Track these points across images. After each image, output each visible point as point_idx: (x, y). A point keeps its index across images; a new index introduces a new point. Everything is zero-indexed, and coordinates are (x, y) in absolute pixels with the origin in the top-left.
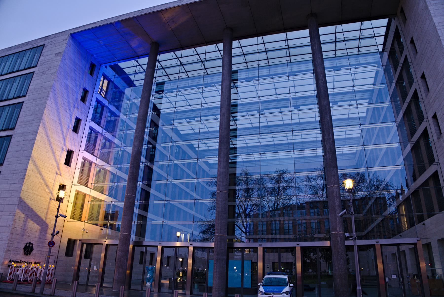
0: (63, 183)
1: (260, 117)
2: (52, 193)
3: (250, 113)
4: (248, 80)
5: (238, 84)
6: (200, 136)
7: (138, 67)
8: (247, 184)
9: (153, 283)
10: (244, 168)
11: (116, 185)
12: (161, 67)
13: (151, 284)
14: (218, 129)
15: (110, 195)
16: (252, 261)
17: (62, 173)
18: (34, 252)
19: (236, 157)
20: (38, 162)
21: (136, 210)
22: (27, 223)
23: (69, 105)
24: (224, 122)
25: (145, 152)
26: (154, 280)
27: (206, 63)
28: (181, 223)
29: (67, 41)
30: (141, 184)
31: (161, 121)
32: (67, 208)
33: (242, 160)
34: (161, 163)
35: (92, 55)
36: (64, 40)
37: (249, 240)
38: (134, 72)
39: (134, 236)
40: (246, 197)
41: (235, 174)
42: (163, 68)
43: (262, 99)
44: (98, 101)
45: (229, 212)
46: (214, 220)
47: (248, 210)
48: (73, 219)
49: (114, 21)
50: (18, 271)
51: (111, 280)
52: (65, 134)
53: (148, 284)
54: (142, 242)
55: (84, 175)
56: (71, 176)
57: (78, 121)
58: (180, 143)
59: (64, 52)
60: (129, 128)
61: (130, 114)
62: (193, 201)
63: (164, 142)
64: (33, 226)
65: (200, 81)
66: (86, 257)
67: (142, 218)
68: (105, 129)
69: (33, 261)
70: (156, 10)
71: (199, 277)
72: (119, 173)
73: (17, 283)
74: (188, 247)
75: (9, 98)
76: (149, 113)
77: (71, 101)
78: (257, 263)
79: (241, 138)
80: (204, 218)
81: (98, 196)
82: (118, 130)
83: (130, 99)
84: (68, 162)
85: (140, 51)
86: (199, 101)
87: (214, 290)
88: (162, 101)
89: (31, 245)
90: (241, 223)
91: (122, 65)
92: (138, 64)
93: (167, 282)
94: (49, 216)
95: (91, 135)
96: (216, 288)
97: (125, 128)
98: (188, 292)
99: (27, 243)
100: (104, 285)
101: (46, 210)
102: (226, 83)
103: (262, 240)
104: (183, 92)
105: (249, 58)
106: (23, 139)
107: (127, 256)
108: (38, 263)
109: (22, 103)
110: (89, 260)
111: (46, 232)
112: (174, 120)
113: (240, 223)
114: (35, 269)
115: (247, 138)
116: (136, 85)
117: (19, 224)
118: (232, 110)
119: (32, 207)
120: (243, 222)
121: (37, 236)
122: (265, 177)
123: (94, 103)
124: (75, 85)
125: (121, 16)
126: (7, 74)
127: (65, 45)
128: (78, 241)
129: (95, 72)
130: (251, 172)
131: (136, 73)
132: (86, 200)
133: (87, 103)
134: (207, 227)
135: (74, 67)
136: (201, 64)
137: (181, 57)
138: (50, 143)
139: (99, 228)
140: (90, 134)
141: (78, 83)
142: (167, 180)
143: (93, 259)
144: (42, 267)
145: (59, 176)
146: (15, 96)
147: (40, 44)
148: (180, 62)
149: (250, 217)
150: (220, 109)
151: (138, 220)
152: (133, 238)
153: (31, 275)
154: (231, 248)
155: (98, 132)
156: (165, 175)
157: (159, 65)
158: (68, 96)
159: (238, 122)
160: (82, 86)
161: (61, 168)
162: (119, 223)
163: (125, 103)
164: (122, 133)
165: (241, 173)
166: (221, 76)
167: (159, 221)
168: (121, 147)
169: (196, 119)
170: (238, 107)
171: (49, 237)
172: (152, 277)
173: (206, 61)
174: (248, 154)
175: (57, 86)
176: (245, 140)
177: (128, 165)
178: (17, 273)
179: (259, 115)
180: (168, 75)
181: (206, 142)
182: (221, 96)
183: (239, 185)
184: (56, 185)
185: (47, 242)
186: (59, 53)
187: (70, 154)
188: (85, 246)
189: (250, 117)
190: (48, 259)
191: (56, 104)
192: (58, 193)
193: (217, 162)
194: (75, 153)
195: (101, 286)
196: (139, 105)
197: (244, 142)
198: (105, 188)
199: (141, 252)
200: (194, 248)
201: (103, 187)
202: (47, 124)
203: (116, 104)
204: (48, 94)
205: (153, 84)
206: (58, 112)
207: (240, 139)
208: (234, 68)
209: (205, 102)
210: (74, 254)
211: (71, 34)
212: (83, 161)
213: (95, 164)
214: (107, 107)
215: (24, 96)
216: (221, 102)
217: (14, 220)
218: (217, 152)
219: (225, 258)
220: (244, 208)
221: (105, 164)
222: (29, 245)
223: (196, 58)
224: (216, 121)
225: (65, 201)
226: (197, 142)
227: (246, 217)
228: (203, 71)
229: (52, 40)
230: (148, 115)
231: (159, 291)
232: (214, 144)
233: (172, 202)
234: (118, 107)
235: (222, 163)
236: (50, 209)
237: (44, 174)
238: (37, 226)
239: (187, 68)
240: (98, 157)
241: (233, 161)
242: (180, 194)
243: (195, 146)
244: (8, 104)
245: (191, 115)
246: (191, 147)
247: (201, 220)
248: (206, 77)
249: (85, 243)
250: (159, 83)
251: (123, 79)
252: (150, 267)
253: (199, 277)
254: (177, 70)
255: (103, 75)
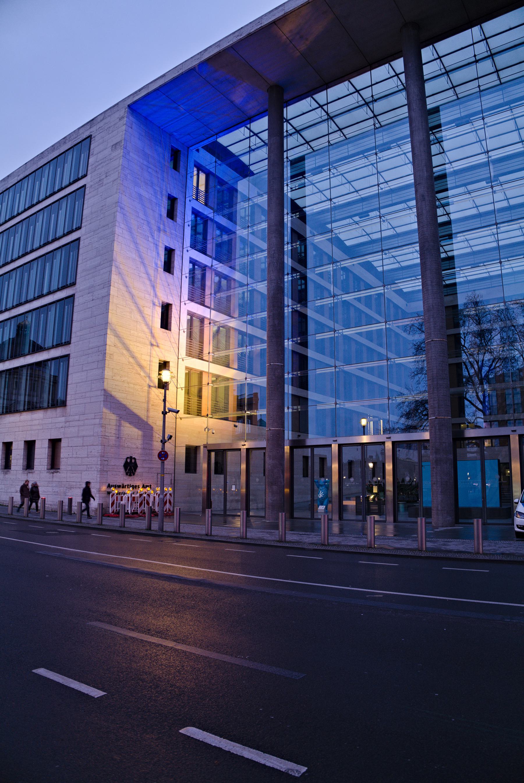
0: (163, 359)
1: (494, 192)
2: (149, 377)
3: (471, 187)
4: (459, 122)
5: (444, 134)
6: (382, 245)
7: (253, 139)
8: (479, 323)
9: (330, 506)
10: (470, 294)
11: (248, 350)
12: (294, 131)
13: (326, 508)
14: (415, 226)
15: (241, 368)
16: (499, 461)
17: (159, 341)
18: (139, 470)
19: (454, 274)
20: (120, 330)
21: (289, 389)
22: (122, 427)
23: (151, 228)
24: (424, 212)
25: (290, 288)
26: (330, 502)
27: (376, 104)
28: (366, 403)
29: (125, 119)
30: (290, 343)
31: (308, 229)
32: (177, 397)
33: (465, 279)
34: (319, 303)
35: (171, 135)
36: (121, 119)
37: (490, 423)
38: (248, 150)
39: (290, 432)
40: (479, 346)
41: (457, 306)
42: (298, 132)
43: (494, 155)
44: (196, 213)
45: (452, 376)
46: (425, 392)
47: (485, 369)
48: (189, 414)
49: (196, 63)
50: (122, 500)
51: (260, 505)
52: (153, 279)
53: (322, 508)
54: (304, 441)
55: (194, 341)
56: (174, 345)
57: (169, 252)
58: (347, 263)
59: (125, 139)
60: (256, 250)
61: (254, 225)
62: (384, 363)
63: (318, 264)
64: (131, 431)
65: (369, 142)
66: (216, 472)
67: (301, 401)
68: (215, 259)
69: (137, 483)
70: (265, 22)
71: (408, 492)
72: (250, 330)
73: (125, 517)
74: (383, 443)
75: (57, 236)
76: (285, 217)
77: (153, 222)
78: (508, 466)
79: (460, 238)
80: (405, 391)
81: (222, 373)
82: (237, 256)
83: (249, 199)
84: (165, 324)
85: (251, 108)
86: (373, 180)
87: (434, 512)
88: (305, 192)
89: (133, 461)
90: (474, 394)
91: (224, 140)
92: (252, 134)
93: (351, 503)
94: (151, 414)
95: (194, 273)
96: (438, 510)
97: (248, 250)
98: (390, 518)
99: (128, 458)
100: (251, 514)
101: (146, 405)
102: (420, 136)
103: (515, 422)
104: (340, 169)
105: (457, 77)
106: (91, 298)
107: (282, 465)
108: (147, 486)
109: (78, 239)
110: (222, 476)
111: (152, 438)
112: (331, 222)
113: (471, 394)
114: (145, 495)
115: (470, 235)
116: (255, 172)
117: (111, 430)
118: (438, 186)
119: (125, 402)
120: (477, 393)
121: (140, 446)
122: (512, 306)
123: (189, 217)
124: (152, 193)
125: (206, 50)
126: (25, 210)
127: (124, 127)
128: (202, 447)
129: (182, 164)
130: (484, 298)
131: (251, 150)
132: (205, 380)
133: (179, 220)
134: (413, 406)
135: (145, 163)
136: (365, 108)
137: (327, 104)
138: (132, 296)
139: (230, 424)
140: (192, 272)
141: (158, 189)
142: (335, 331)
143: (228, 474)
144: (155, 491)
145: (156, 348)
146: (66, 232)
147: (85, 137)
148: (327, 113)
149: (489, 382)
150: (414, 189)
151: (292, 405)
152: (289, 435)
153: (141, 504)
154: (459, 439)
155: (206, 266)
156: (330, 323)
157: (290, 127)
158: (145, 214)
159: (451, 209)
160: (164, 192)
161: (156, 335)
162: (261, 412)
163: (242, 208)
164: (245, 260)
165: (465, 304)
166: (408, 125)
167: (329, 404)
168: (248, 285)
169: (372, 214)
170: (448, 179)
171: (157, 446)
172: (326, 496)
173: (376, 101)
174: (475, 266)
175: (126, 200)
176: (467, 240)
177: (265, 314)
178: (122, 502)
179: (492, 187)
180: (307, 143)
181: (394, 254)
182: (414, 163)
183: (464, 325)
184: (153, 364)
185: (156, 453)
186: (116, 144)
187: (166, 309)
188: (213, 454)
189: (473, 194)
190: (163, 479)
191: (130, 231)
192: (159, 374)
193: (421, 287)
194: (173, 307)
195: (248, 515)
196: (266, 207)
197: (465, 244)
198: (231, 357)
199: (304, 457)
200: (394, 443)
201: (228, 356)
202: (121, 266)
203: (226, 211)
204: (115, 217)
205: (285, 164)
206: (136, 243)
207: (459, 239)
208: (431, 103)
209: (383, 181)
210: (198, 468)
211: (129, 106)
212: (189, 317)
213: (210, 319)
214: (212, 220)
215: (79, 228)
216: (415, 174)
217: (102, 426)
218: (419, 270)
219: (451, 457)
220: (476, 367)
221: (225, 317)
222: (131, 461)
223: (354, 100)
224: (408, 212)
225: (171, 387)
226: (378, 256)
227: (481, 383)
228: (371, 122)
229: (102, 124)
230: (285, 220)
231: (341, 518)
232: (411, 256)
233: (347, 368)
234: (231, 217)
235: (430, 288)
236: (151, 403)
237: (132, 348)
238: (136, 430)
239: (341, 121)
240: (212, 307)
241: (448, 282)
242: (358, 352)
243: (375, 264)
244: (58, 246)
245: (361, 208)
246: (369, 267)
247: (401, 394)
248: (379, 132)
249: (213, 451)
250: (295, 159)
251: (230, 166)
252: (323, 480)
253: (408, 492)
254: (323, 128)
255: (195, 166)
